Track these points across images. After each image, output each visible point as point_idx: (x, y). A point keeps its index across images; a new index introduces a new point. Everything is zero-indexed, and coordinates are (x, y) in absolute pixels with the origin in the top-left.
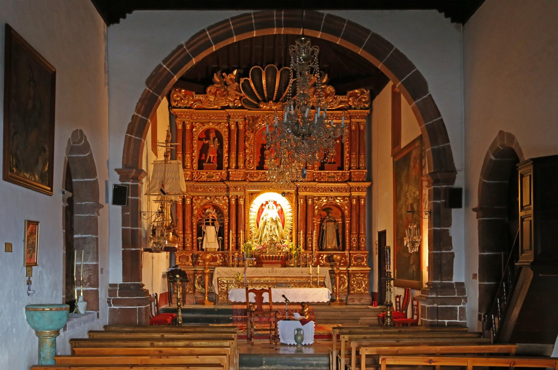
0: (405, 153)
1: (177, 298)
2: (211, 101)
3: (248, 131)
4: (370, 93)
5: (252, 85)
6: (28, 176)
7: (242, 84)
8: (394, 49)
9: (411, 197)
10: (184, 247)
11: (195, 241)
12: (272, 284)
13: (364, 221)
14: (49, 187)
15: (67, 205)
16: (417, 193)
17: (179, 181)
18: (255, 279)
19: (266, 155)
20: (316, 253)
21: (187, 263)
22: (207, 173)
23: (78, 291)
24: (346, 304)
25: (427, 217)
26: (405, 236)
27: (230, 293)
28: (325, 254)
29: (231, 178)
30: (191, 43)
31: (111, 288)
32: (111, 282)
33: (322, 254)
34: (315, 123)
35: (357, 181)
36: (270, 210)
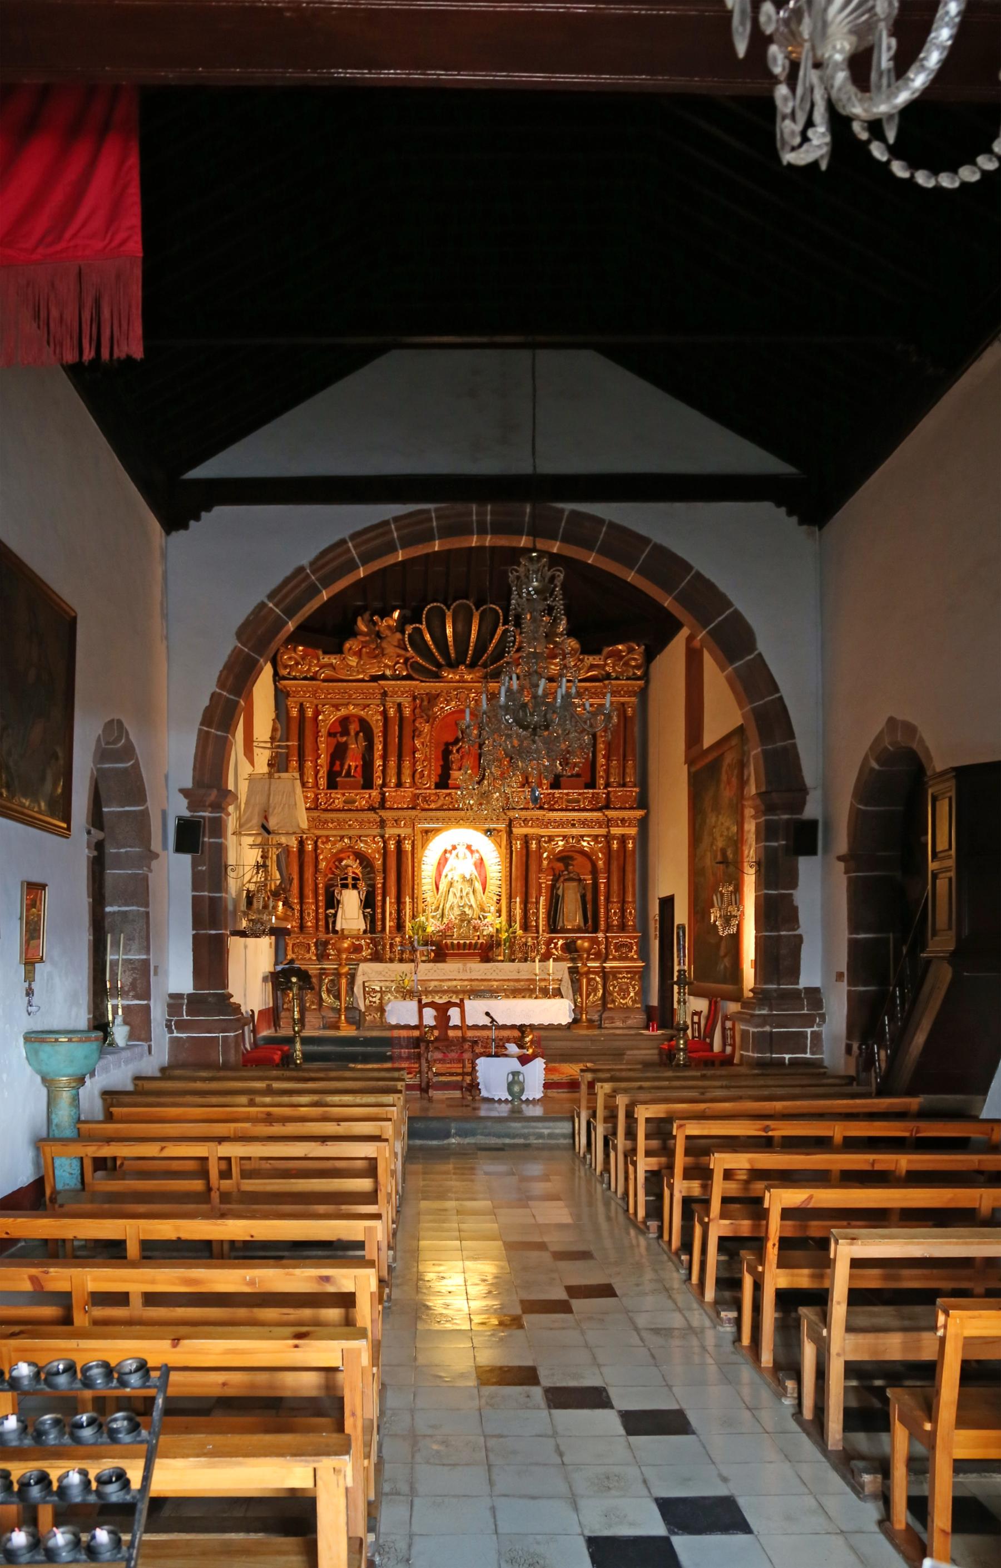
0: (710, 758)
1: (294, 1019)
2: (351, 667)
3: (419, 720)
4: (646, 650)
5: (428, 637)
6: (27, 803)
7: (409, 635)
8: (693, 572)
9: (721, 836)
10: (302, 927)
11: (321, 916)
12: (464, 992)
13: (634, 880)
14: (65, 822)
15: (95, 853)
16: (734, 829)
17: (295, 810)
18: (433, 984)
19: (452, 762)
20: (544, 936)
21: (307, 956)
22: (343, 794)
23: (113, 1006)
24: (600, 1027)
25: (753, 871)
26: (713, 906)
27: (387, 1008)
28: (562, 938)
29: (388, 804)
30: (320, 563)
31: (172, 1001)
32: (173, 989)
33: (555, 938)
34: (558, 705)
35: (620, 808)
36: (461, 864)
